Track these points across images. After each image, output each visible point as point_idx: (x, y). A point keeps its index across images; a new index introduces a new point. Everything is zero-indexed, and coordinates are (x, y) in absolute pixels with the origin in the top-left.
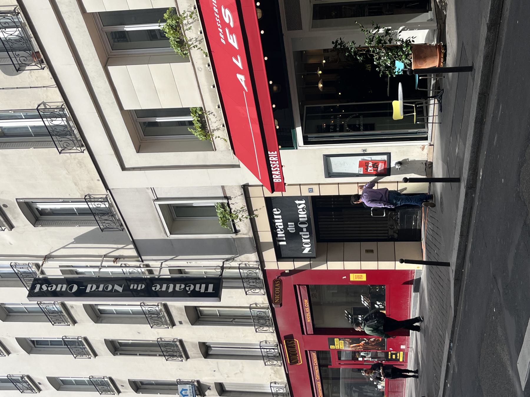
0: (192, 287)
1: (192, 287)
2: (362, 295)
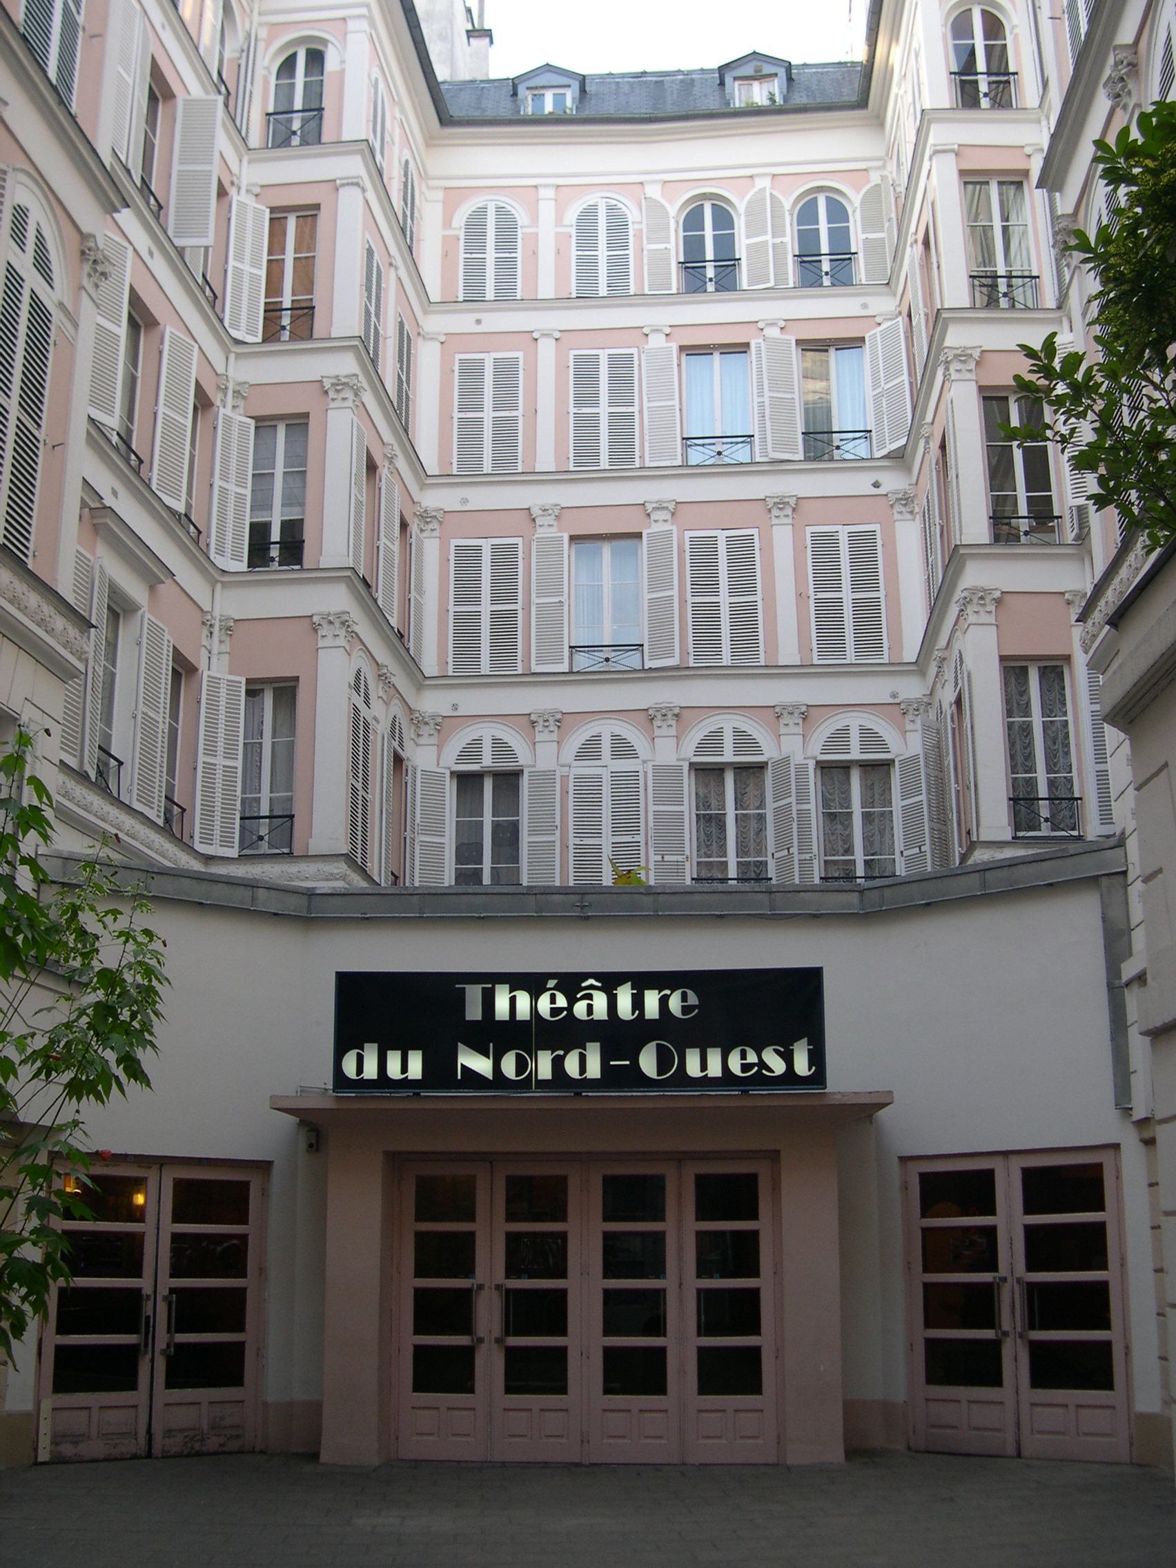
1: (544, 1005)
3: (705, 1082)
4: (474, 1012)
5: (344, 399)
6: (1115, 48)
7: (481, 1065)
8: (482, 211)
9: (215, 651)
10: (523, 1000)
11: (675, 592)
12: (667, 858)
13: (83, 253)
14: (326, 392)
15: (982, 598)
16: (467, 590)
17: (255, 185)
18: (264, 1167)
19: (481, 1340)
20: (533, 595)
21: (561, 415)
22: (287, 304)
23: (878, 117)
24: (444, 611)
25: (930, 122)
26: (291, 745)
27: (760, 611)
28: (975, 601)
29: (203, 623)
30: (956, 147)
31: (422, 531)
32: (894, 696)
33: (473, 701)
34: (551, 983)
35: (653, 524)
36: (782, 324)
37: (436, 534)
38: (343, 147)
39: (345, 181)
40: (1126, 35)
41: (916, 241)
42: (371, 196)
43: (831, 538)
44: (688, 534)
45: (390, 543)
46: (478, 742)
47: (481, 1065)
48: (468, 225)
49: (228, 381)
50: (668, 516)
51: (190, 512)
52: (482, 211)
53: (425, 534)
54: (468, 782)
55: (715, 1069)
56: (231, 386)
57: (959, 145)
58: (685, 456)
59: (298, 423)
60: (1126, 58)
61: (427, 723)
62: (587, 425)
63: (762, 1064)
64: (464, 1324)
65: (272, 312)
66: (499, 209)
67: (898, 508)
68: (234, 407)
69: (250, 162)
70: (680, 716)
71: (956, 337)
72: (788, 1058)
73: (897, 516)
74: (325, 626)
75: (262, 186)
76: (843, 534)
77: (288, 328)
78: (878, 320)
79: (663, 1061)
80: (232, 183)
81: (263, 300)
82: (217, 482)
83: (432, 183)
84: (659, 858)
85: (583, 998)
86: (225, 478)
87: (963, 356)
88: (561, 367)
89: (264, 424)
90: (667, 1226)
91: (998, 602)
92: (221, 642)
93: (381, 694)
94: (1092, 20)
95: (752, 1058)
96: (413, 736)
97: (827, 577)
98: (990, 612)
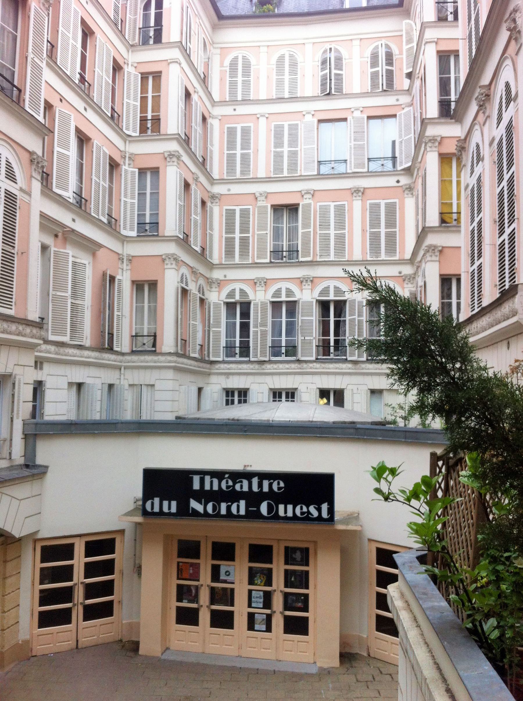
0: (224, 486)
1: (224, 486)
2: (385, 307)
3: (286, 518)
4: (196, 486)
5: (173, 162)
6: (480, 87)
7: (198, 507)
8: (236, 58)
9: (125, 269)
10: (216, 481)
11: (311, 230)
12: (306, 338)
13: (31, 161)
14: (166, 159)
15: (433, 250)
16: (230, 228)
17: (134, 62)
18: (122, 532)
19: (202, 606)
20: (256, 230)
21: (268, 152)
22: (149, 117)
23: (408, 10)
24: (221, 237)
25: (425, 28)
26: (155, 307)
27: (347, 237)
28: (430, 251)
29: (119, 259)
30: (436, 40)
31: (212, 203)
32: (400, 273)
33: (232, 274)
34: (227, 476)
35: (304, 200)
36: (361, 109)
37: (218, 204)
38: (171, 45)
39: (172, 61)
40: (486, 80)
41: (418, 77)
42: (185, 65)
43: (378, 205)
44: (319, 204)
45: (197, 217)
46: (234, 291)
47: (198, 507)
48: (231, 65)
49: (126, 153)
50: (311, 196)
51: (112, 213)
52: (236, 58)
53: (213, 204)
54: (230, 306)
55: (290, 514)
56: (127, 155)
57: (438, 39)
58: (319, 169)
59: (155, 171)
60: (485, 92)
61: (214, 283)
62: (278, 156)
63: (309, 512)
64: (195, 599)
65: (144, 120)
66: (244, 57)
67: (406, 192)
68: (129, 164)
69: (132, 51)
70: (312, 281)
71: (431, 131)
72: (319, 510)
73: (406, 196)
74: (167, 259)
75: (138, 63)
76: (383, 203)
77: (150, 128)
78: (403, 106)
79: (270, 508)
80: (125, 63)
81: (139, 115)
82: (123, 199)
83: (215, 46)
84: (303, 338)
85: (239, 482)
86: (126, 196)
87: (433, 140)
88: (269, 130)
89: (142, 172)
90: (273, 566)
91: (441, 252)
92: (127, 265)
93: (193, 279)
94: (478, 49)
95: (305, 509)
96: (209, 288)
97: (375, 222)
98: (436, 256)
